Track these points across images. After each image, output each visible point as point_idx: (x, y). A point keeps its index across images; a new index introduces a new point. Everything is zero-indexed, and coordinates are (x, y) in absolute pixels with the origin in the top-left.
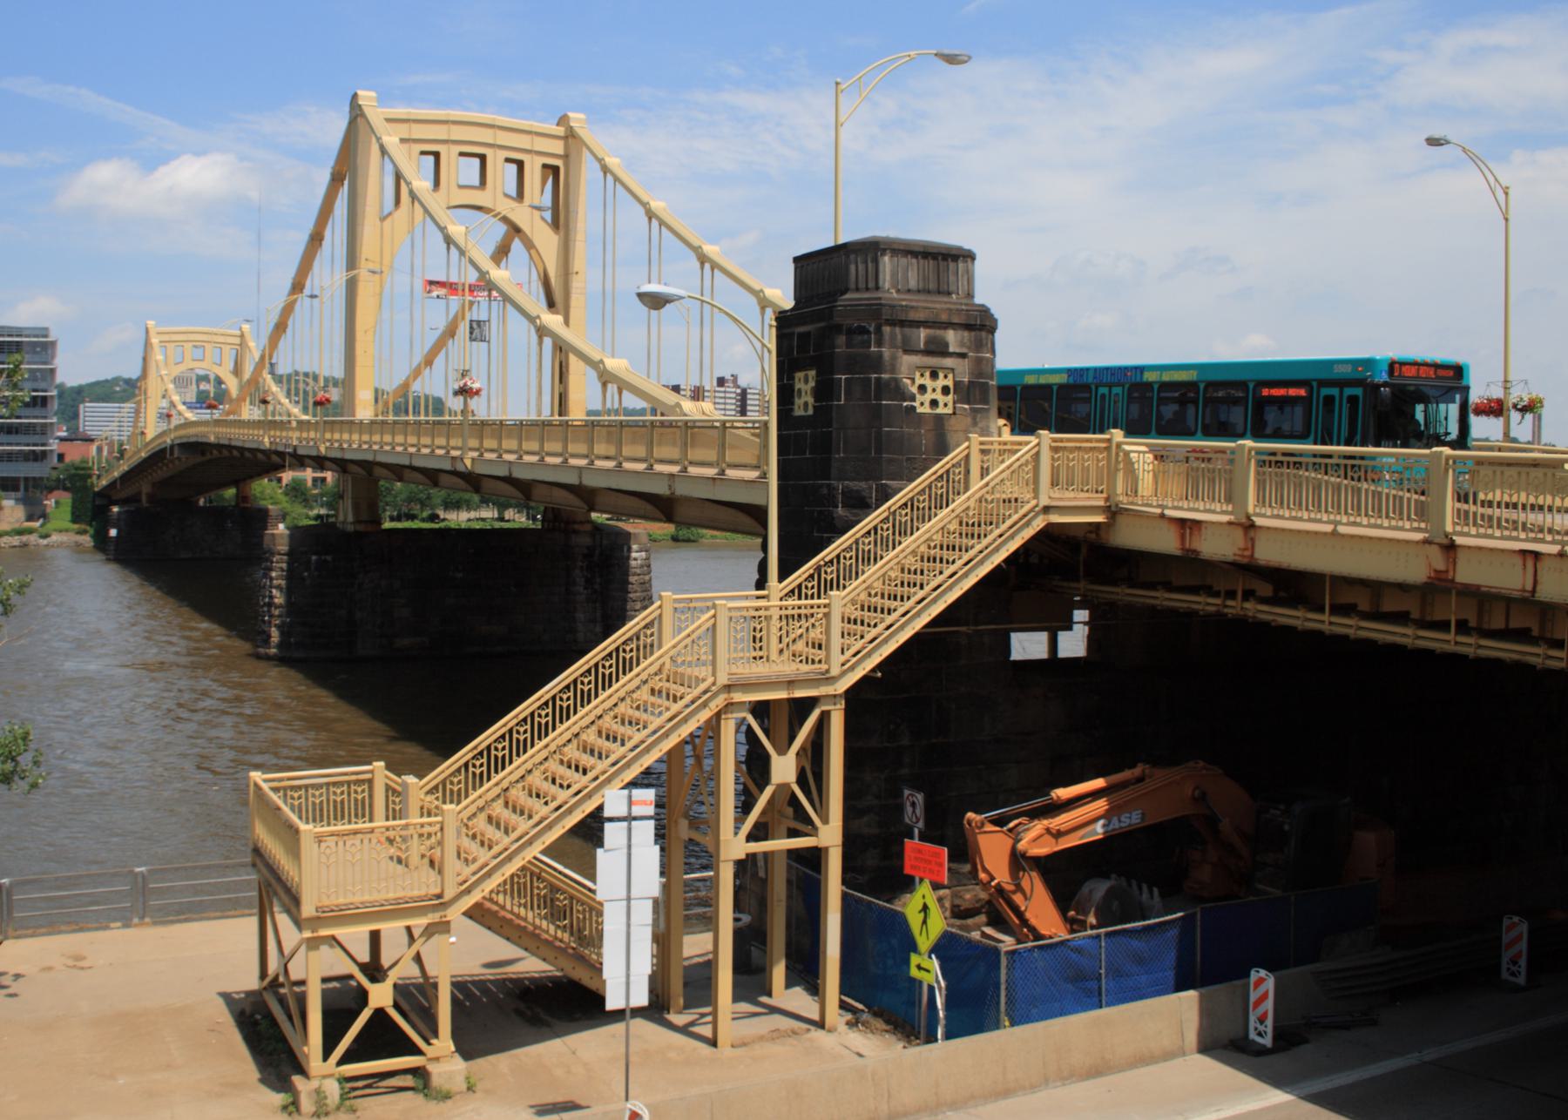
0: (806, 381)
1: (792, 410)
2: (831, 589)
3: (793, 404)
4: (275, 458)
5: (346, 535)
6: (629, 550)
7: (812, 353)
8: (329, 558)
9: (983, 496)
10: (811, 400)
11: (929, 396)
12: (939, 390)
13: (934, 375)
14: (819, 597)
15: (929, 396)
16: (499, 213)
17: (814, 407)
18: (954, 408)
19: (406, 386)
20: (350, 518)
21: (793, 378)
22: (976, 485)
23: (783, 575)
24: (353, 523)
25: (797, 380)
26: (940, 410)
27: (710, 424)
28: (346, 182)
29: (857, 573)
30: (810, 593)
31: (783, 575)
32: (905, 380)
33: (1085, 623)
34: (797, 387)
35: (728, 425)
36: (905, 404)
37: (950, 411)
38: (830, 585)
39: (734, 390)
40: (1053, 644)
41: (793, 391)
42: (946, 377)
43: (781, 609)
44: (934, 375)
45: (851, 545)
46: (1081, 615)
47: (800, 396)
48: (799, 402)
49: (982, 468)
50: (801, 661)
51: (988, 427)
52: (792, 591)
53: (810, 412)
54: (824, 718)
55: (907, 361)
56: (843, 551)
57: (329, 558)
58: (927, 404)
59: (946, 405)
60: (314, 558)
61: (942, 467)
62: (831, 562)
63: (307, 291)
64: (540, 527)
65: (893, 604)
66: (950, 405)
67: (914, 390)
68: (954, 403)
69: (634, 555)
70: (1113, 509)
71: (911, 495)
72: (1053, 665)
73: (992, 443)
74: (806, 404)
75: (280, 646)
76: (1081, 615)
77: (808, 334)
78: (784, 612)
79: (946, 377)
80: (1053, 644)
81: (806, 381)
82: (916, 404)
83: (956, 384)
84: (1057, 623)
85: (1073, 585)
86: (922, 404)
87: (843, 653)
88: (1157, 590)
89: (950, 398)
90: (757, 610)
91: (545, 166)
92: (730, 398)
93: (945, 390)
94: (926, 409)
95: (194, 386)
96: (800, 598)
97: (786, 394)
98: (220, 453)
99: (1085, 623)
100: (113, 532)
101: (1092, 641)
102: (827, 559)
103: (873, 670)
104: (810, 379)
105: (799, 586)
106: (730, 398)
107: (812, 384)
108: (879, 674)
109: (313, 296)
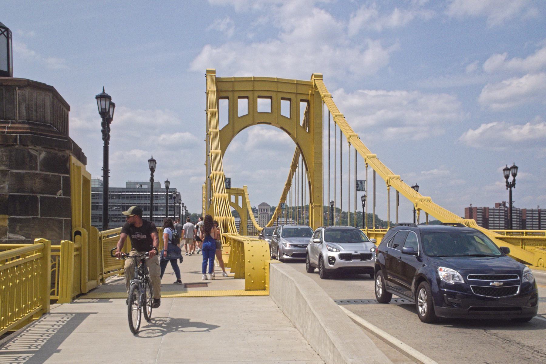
39: (503, 209)
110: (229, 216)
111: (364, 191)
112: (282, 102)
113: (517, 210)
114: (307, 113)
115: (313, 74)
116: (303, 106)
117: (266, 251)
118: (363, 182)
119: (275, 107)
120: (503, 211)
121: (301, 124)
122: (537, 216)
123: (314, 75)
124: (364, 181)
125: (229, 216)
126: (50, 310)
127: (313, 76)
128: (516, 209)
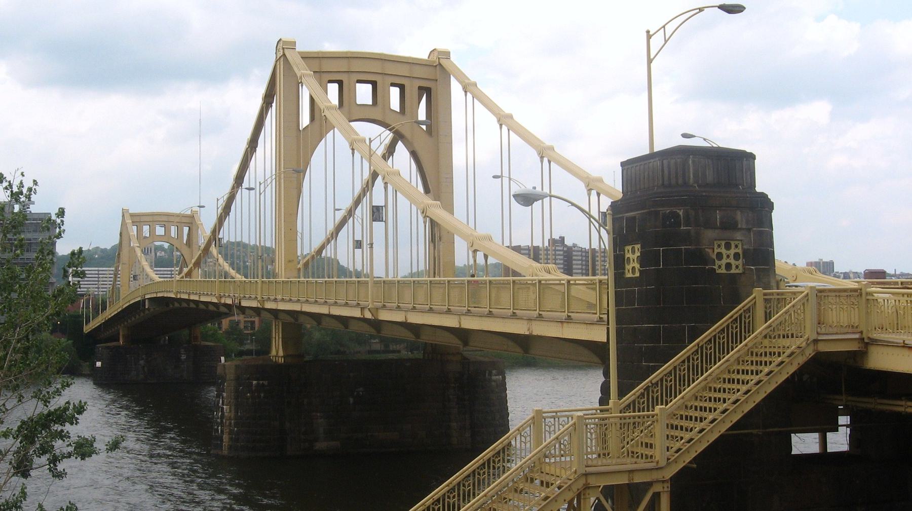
0: (633, 252)
1: (624, 273)
2: (657, 405)
3: (624, 269)
4: (223, 309)
5: (280, 365)
6: (490, 374)
7: (661, 267)
8: (266, 383)
9: (768, 333)
10: (637, 266)
11: (724, 261)
12: (732, 257)
13: (728, 247)
14: (648, 411)
15: (724, 261)
16: (393, 128)
17: (640, 271)
18: (744, 269)
19: (320, 251)
20: (281, 353)
21: (624, 251)
22: (761, 328)
23: (622, 393)
24: (284, 357)
25: (626, 251)
26: (733, 271)
27: (558, 282)
28: (274, 105)
29: (689, 381)
30: (641, 407)
31: (622, 393)
32: (707, 250)
33: (847, 426)
34: (627, 256)
35: (571, 282)
36: (707, 267)
37: (740, 272)
38: (655, 402)
39: (562, 248)
40: (824, 442)
41: (624, 258)
42: (736, 246)
43: (621, 419)
44: (728, 247)
45: (671, 371)
46: (844, 420)
47: (629, 264)
48: (628, 267)
49: (766, 312)
50: (638, 456)
51: (769, 282)
52: (629, 405)
53: (637, 274)
54: (657, 496)
55: (709, 234)
56: (665, 375)
57: (266, 383)
58: (723, 267)
59: (737, 267)
60: (254, 382)
61: (736, 313)
62: (657, 384)
63: (245, 184)
64: (422, 357)
65: (704, 414)
66: (740, 267)
67: (714, 257)
68: (743, 265)
69: (494, 378)
70: (866, 341)
71: (714, 334)
72: (824, 458)
73: (772, 294)
74: (633, 268)
75: (230, 448)
76: (844, 420)
77: (634, 218)
78: (623, 421)
79: (736, 246)
80: (824, 442)
81: (633, 252)
82: (716, 267)
83: (745, 252)
84: (828, 425)
85: (837, 397)
86: (720, 267)
87: (668, 450)
88: (902, 400)
89: (740, 262)
90: (603, 420)
91: (420, 88)
92: (559, 255)
93: (737, 256)
94: (723, 271)
95: (153, 254)
96: (634, 411)
97: (620, 262)
98: (189, 305)
99: (847, 426)
100: (99, 364)
101: (854, 439)
102: (653, 382)
103: (690, 462)
104: (636, 250)
105: (634, 402)
106: (559, 255)
107: (638, 254)
108: (695, 466)
109: (250, 189)
110: (146, 248)
111: (382, 221)
112: (172, 227)
113: (581, 251)
114: (189, 234)
115: (280, 40)
116: (186, 230)
117: (793, 277)
118: (381, 208)
119: (167, 231)
120: (562, 253)
121: (185, 242)
122: (575, 260)
123: (283, 41)
124: (382, 206)
125: (146, 248)
126: (614, 189)
127: (281, 42)
128: (580, 249)
